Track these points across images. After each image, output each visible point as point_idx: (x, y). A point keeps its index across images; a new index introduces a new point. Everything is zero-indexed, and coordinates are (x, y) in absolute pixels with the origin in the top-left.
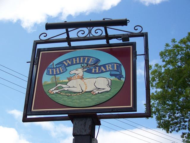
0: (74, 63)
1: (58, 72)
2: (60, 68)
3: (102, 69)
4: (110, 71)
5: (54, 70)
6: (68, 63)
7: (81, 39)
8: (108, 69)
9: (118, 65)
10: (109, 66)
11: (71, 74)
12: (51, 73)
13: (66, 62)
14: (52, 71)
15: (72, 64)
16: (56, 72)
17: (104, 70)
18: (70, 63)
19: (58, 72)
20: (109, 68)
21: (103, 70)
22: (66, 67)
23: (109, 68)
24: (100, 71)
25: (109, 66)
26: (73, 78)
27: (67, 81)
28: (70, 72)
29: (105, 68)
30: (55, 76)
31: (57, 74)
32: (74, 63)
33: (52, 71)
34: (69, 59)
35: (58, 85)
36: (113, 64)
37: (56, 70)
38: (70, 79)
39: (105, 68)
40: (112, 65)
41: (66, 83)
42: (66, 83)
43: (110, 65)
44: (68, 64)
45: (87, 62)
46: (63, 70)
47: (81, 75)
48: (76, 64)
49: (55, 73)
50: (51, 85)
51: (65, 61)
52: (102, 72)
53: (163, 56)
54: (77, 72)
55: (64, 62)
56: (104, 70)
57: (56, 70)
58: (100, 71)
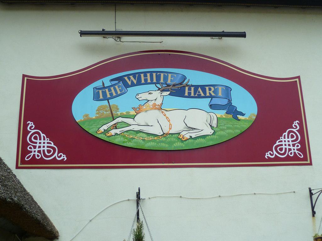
0: (143, 81)
1: (114, 94)
2: (116, 87)
3: (199, 92)
4: (211, 97)
5: (107, 90)
6: (132, 81)
7: (111, 36)
8: (208, 94)
9: (166, 74)
10: (210, 89)
11: (140, 99)
12: (101, 97)
13: (129, 79)
14: (104, 94)
15: (139, 83)
16: (111, 94)
17: (203, 95)
18: (135, 82)
19: (114, 94)
20: (210, 93)
21: (201, 94)
22: (127, 86)
23: (210, 93)
24: (196, 95)
25: (210, 89)
26: (144, 108)
27: (133, 113)
28: (138, 95)
29: (204, 92)
30: (109, 102)
31: (112, 97)
32: (143, 81)
33: (104, 94)
34: (134, 75)
35: (120, 120)
36: (158, 74)
37: (110, 90)
38: (138, 110)
39: (204, 91)
40: (214, 88)
41: (133, 117)
42: (133, 117)
43: (213, 89)
44: (132, 82)
45: (141, 76)
46: (120, 91)
47: (159, 102)
48: (146, 83)
49: (109, 96)
50: (101, 120)
51: (128, 76)
52: (199, 97)
53: (44, 227)
54: (150, 97)
55: (126, 78)
56: (203, 95)
57: (110, 90)
58: (196, 95)
